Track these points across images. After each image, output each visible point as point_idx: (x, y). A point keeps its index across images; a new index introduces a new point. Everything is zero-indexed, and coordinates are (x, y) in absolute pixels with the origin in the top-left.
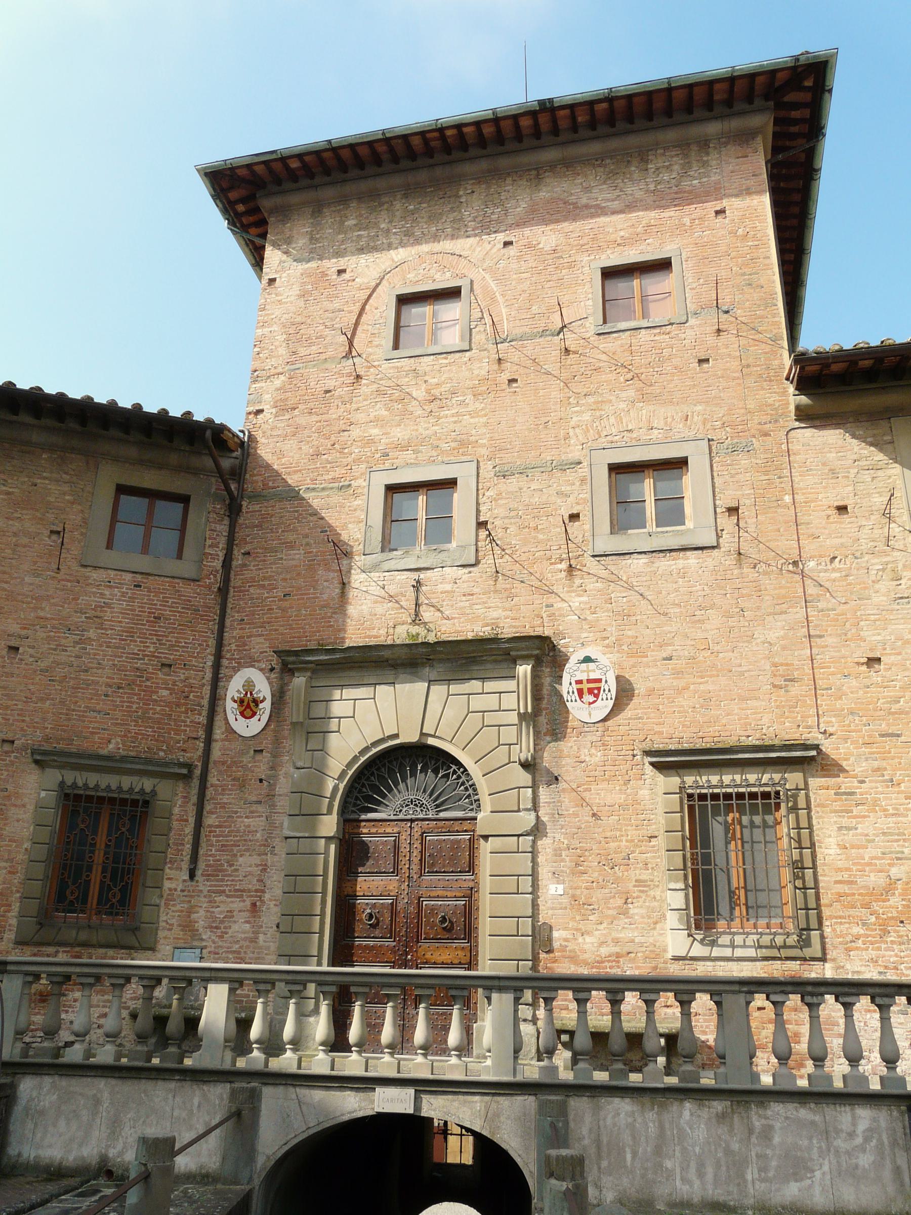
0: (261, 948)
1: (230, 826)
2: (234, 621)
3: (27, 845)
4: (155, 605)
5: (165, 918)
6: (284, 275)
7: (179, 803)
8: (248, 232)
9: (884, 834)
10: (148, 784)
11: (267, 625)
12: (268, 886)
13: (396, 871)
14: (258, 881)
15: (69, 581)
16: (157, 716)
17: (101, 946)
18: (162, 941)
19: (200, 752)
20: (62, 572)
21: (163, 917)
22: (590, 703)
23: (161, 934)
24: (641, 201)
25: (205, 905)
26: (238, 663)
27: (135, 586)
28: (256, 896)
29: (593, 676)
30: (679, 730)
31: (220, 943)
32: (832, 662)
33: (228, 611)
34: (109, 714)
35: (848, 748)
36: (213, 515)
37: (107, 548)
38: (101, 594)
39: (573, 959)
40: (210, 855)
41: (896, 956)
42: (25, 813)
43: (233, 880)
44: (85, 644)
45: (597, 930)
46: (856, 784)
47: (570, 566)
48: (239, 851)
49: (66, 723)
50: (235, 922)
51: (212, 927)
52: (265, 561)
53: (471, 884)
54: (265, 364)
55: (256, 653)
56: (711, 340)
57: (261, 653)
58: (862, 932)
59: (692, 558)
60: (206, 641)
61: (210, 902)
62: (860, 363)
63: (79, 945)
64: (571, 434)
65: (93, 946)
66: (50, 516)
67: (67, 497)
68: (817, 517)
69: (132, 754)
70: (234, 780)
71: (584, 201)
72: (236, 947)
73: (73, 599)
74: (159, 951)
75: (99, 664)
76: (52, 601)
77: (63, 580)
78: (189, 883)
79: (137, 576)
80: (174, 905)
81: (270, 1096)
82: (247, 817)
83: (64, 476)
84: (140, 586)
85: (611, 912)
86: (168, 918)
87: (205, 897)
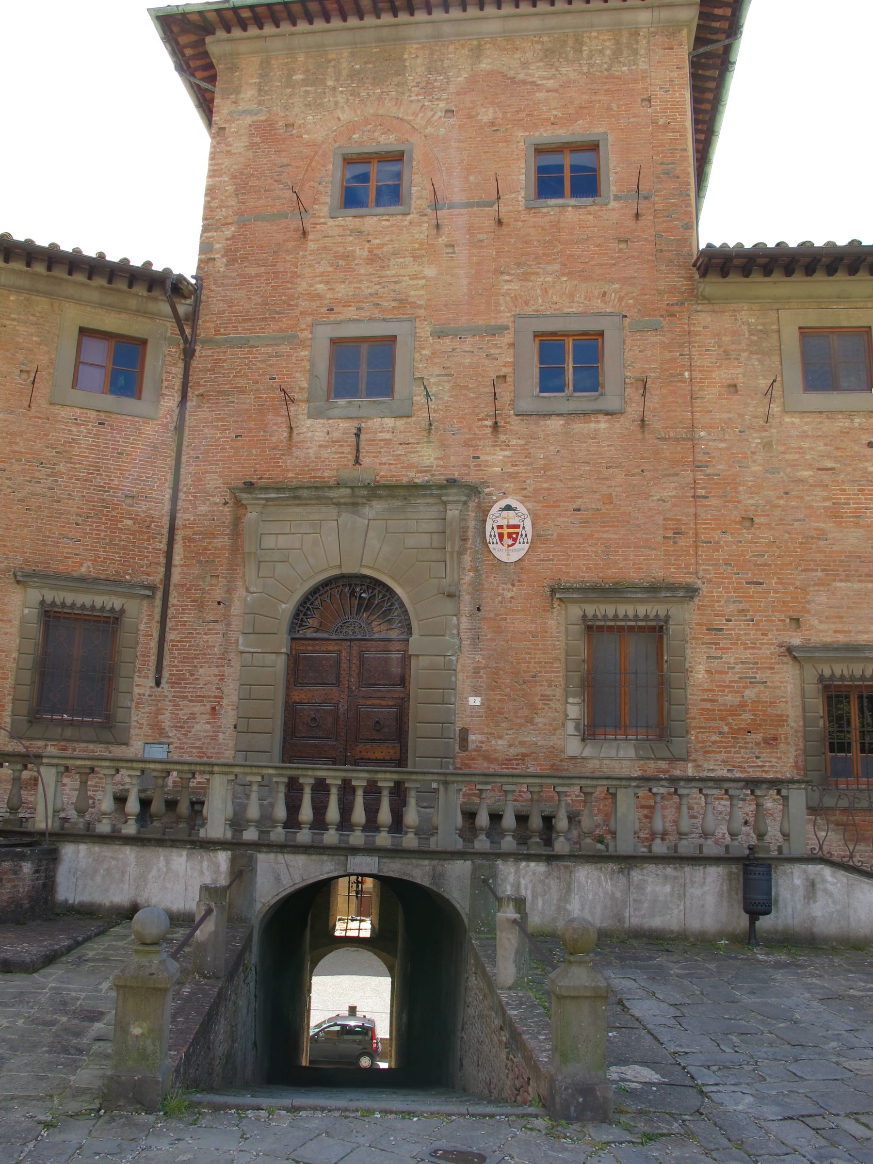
0: (220, 744)
1: (190, 642)
2: (189, 458)
3: (15, 655)
4: (118, 441)
5: (136, 719)
6: (233, 125)
7: (145, 620)
8: (194, 76)
9: (742, 663)
10: (117, 603)
11: (220, 463)
12: (225, 693)
13: (338, 683)
14: (217, 688)
15: (39, 418)
16: (123, 543)
17: (84, 742)
18: (134, 738)
19: (161, 576)
20: (33, 408)
21: (134, 718)
22: (509, 546)
23: (133, 732)
24: (574, 81)
25: (170, 708)
26: (195, 497)
27: (99, 423)
28: (215, 702)
29: (512, 522)
30: (582, 569)
31: (185, 740)
32: (713, 520)
33: (184, 448)
34: (80, 541)
35: (721, 592)
36: (169, 359)
37: (73, 388)
38: (69, 430)
39: (487, 758)
40: (174, 666)
41: (743, 758)
42: (11, 627)
43: (194, 688)
44: (56, 476)
45: (507, 734)
46: (724, 622)
47: (496, 423)
48: (200, 662)
49: (42, 548)
50: (197, 723)
51: (177, 727)
52: (217, 403)
53: (402, 696)
54: (215, 213)
55: (210, 488)
56: (631, 223)
57: (216, 488)
58: (718, 739)
59: (603, 424)
60: (164, 476)
61: (174, 705)
62: (758, 260)
63: (64, 740)
64: (501, 301)
65: (77, 741)
66: (20, 356)
67: (35, 339)
68: (710, 393)
69: (102, 577)
70: (192, 601)
71: (521, 76)
72: (198, 744)
73: (45, 435)
74: (132, 746)
75: (70, 495)
76: (25, 437)
77: (35, 417)
78: (155, 689)
79: (101, 414)
80: (143, 708)
81: (264, 861)
82: (205, 634)
83: (31, 318)
84: (104, 424)
85: (519, 721)
86: (138, 719)
87: (170, 701)
